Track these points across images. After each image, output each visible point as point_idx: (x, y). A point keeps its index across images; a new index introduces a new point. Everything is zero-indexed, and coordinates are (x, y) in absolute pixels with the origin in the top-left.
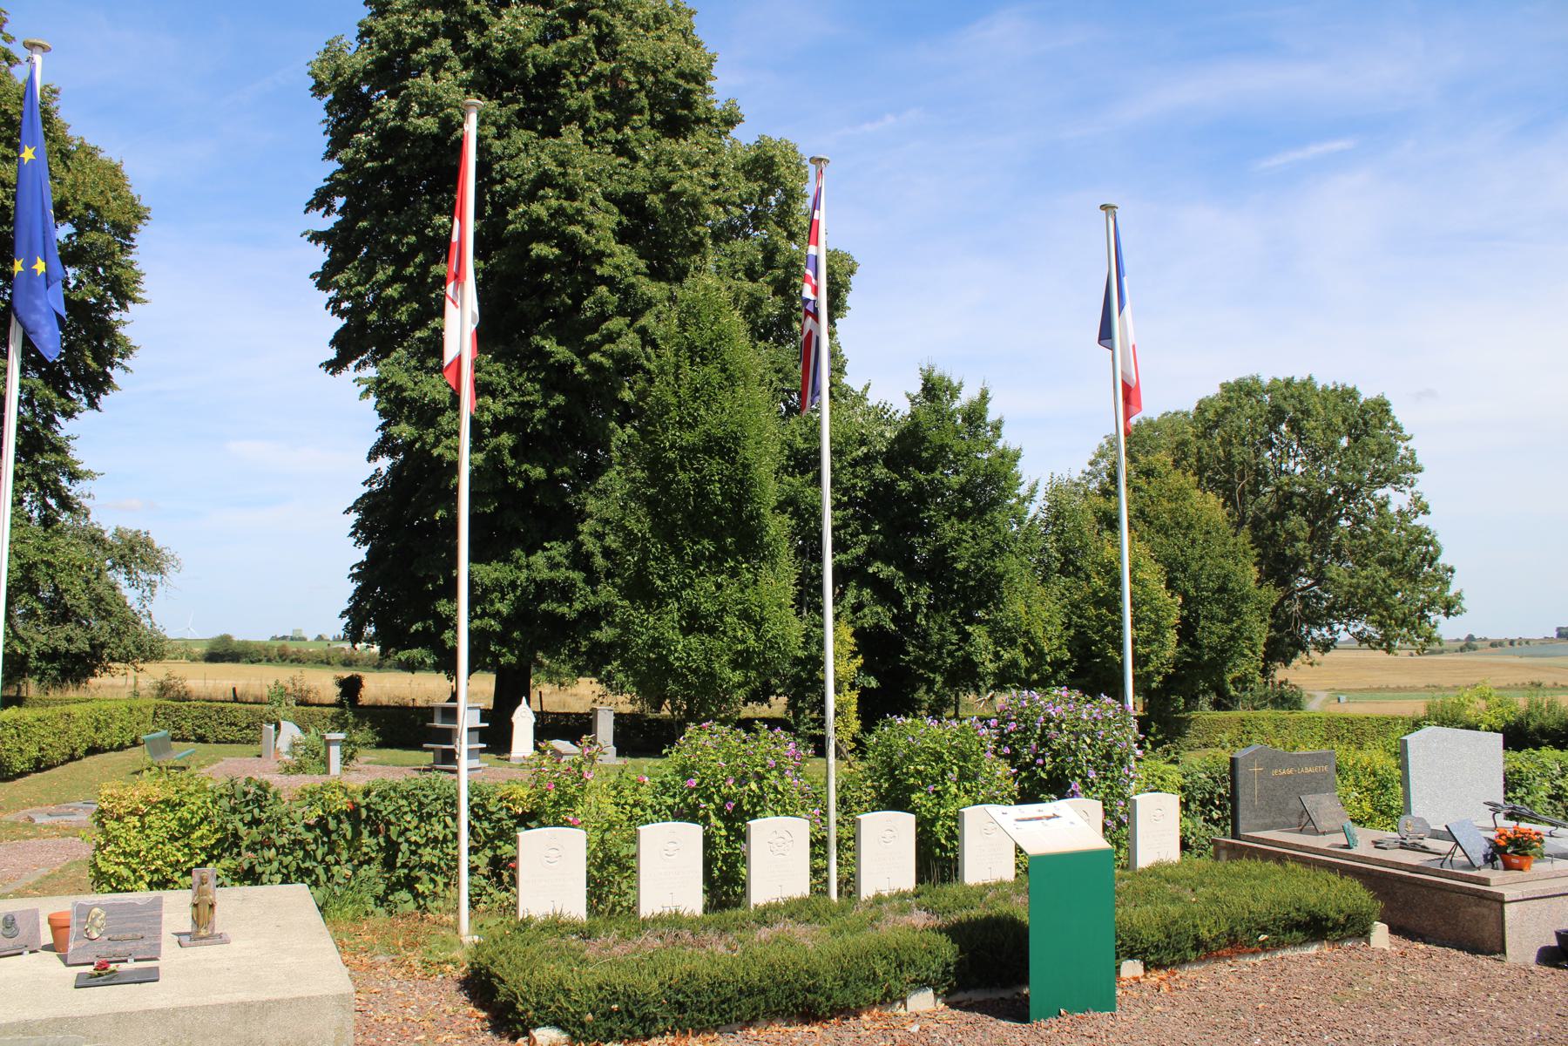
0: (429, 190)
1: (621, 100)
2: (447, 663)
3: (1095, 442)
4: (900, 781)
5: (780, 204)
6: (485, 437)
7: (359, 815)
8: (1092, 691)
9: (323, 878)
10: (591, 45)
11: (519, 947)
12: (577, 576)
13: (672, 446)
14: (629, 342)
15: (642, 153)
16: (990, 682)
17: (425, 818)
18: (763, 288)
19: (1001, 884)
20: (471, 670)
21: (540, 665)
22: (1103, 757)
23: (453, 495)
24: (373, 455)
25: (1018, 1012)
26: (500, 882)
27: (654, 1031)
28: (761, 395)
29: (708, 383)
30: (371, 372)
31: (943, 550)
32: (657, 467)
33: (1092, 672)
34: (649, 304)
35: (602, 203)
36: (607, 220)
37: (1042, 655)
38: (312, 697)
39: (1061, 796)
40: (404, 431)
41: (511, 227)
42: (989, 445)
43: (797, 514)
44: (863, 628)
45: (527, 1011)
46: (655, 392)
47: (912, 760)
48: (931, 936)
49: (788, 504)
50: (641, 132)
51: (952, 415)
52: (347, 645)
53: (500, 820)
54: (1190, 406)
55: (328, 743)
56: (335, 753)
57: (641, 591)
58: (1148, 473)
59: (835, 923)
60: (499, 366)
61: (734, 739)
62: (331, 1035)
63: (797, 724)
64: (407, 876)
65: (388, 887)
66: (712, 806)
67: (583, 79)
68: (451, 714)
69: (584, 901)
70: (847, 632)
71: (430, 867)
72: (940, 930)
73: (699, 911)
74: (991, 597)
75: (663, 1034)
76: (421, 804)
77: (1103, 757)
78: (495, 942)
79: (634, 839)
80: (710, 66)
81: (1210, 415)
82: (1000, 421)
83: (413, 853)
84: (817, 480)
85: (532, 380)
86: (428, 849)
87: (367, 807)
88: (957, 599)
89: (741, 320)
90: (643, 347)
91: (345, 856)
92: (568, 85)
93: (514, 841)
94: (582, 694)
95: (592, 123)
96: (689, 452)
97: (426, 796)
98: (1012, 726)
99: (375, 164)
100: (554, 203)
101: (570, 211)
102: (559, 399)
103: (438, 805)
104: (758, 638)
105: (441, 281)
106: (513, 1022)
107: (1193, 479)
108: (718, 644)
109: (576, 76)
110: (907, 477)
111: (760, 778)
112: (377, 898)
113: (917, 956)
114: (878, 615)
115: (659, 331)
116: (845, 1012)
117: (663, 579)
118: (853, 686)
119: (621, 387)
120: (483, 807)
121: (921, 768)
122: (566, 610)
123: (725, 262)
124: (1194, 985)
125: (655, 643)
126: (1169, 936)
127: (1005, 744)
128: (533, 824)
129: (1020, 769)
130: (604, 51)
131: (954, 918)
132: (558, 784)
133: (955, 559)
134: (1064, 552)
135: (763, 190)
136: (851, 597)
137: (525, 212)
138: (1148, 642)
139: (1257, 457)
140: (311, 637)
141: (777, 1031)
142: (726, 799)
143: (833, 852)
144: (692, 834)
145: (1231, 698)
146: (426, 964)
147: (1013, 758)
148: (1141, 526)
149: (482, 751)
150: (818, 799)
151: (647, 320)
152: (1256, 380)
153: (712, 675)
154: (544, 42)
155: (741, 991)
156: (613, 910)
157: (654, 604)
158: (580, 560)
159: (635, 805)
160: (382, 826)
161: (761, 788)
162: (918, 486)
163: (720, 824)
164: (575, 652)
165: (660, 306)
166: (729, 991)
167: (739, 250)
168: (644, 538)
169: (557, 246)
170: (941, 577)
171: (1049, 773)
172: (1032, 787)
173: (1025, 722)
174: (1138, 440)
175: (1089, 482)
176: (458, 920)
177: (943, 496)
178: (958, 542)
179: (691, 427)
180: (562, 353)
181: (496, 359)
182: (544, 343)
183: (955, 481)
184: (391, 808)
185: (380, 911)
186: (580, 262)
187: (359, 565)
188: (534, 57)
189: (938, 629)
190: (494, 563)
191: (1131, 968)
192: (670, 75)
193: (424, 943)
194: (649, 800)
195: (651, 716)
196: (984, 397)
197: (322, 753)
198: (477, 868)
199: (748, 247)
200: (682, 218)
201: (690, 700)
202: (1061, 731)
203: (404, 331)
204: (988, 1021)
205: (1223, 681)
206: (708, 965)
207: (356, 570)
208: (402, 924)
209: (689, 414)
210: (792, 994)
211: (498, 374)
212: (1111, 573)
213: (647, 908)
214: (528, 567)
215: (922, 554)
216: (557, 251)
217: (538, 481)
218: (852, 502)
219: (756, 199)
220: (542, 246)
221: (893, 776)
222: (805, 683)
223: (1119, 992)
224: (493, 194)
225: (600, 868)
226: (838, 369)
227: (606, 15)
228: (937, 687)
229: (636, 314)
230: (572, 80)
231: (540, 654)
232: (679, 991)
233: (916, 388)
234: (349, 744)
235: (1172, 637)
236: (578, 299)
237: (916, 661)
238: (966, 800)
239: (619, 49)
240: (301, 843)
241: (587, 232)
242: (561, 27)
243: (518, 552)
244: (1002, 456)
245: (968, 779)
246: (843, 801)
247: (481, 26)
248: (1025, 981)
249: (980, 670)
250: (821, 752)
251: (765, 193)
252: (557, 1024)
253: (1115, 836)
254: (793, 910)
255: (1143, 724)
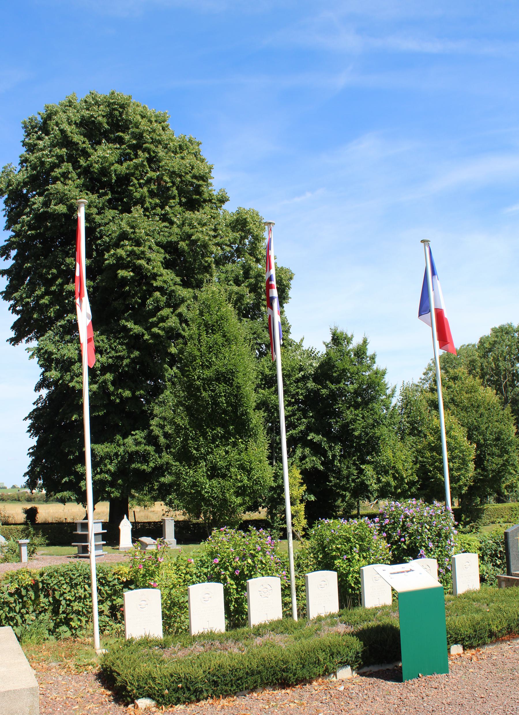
0: (62, 244)
1: (163, 192)
2: (82, 499)
3: (426, 362)
4: (328, 554)
5: (251, 243)
6: (98, 376)
7: (38, 586)
8: (429, 501)
9: (20, 621)
10: (145, 163)
11: (127, 655)
12: (151, 449)
13: (199, 378)
14: (173, 322)
15: (175, 220)
16: (376, 494)
17: (74, 586)
18: (244, 289)
19: (384, 607)
20: (95, 502)
21: (133, 497)
22: (436, 536)
23: (81, 407)
24: (38, 388)
25: (397, 676)
26: (116, 619)
27: (201, 697)
28: (245, 349)
29: (216, 343)
30: (34, 344)
31: (346, 425)
32: (191, 390)
33: (429, 489)
34: (183, 301)
35: (155, 247)
36: (158, 257)
37: (403, 479)
38: (11, 520)
39: (415, 558)
40: (54, 374)
41: (107, 262)
42: (369, 367)
43: (267, 410)
44: (306, 469)
45: (133, 690)
46: (188, 349)
47: (334, 542)
48: (348, 638)
49: (262, 405)
50: (175, 209)
51: (349, 352)
52: (29, 491)
53: (114, 585)
54: (476, 341)
55: (20, 545)
56: (24, 550)
57: (185, 456)
58: (455, 378)
59: (296, 633)
60: (104, 337)
61: (238, 536)
62: (27, 710)
63: (273, 522)
64: (65, 618)
65: (55, 624)
66: (228, 573)
67: (141, 181)
68: (85, 526)
69: (161, 627)
70: (297, 473)
71: (78, 613)
72: (352, 634)
73: (223, 630)
74: (374, 449)
75: (206, 699)
76: (71, 579)
77: (436, 536)
78: (114, 653)
79: (187, 593)
80: (210, 172)
81: (487, 345)
82: (374, 355)
83: (68, 605)
84: (276, 392)
85: (121, 344)
86: (76, 603)
87: (42, 582)
88: (356, 451)
89: (233, 309)
90: (181, 324)
91: (31, 609)
92: (134, 185)
93: (122, 597)
94: (156, 511)
95: (147, 205)
96: (208, 381)
97: (74, 575)
98: (387, 521)
99: (33, 232)
100: (129, 248)
101: (138, 252)
102: (137, 353)
103: (81, 579)
104: (249, 479)
105: (72, 293)
106: (126, 696)
107: (478, 380)
108: (228, 483)
109: (138, 180)
110: (325, 387)
111: (253, 556)
112: (50, 630)
113: (341, 649)
114: (314, 462)
115: (189, 315)
116: (303, 681)
117: (197, 450)
118: (302, 501)
119: (170, 346)
120: (104, 578)
121: (339, 546)
122: (145, 467)
123: (223, 276)
124: (490, 656)
125: (194, 485)
126: (475, 631)
127: (384, 531)
128: (132, 587)
129: (392, 544)
130: (153, 166)
131: (360, 627)
132: (144, 565)
133: (353, 430)
134: (411, 423)
135: (241, 237)
136: (299, 452)
137: (114, 254)
138: (459, 469)
139: (512, 366)
140: (9, 486)
141: (268, 693)
142: (235, 569)
143: (293, 594)
144: (218, 588)
145: (505, 496)
146: (78, 666)
147: (388, 538)
148: (452, 407)
149: (104, 545)
150: (284, 565)
151: (182, 309)
152: (510, 326)
153: (225, 500)
154: (120, 162)
155: (247, 673)
156: (177, 632)
157: (193, 463)
158: (152, 440)
159: (187, 573)
160: (51, 592)
161: (254, 562)
162: (332, 391)
163: (232, 582)
164: (151, 490)
165: (189, 302)
166: (241, 674)
167: (230, 270)
168: (186, 428)
169: (131, 271)
170: (346, 440)
171: (408, 546)
172: (399, 554)
173: (394, 518)
174: (447, 363)
175: (424, 384)
176: (94, 641)
177: (346, 396)
178: (355, 420)
179: (208, 367)
180: (137, 329)
181: (101, 334)
182: (126, 324)
183: (351, 388)
184: (55, 582)
185: (52, 637)
186: (144, 279)
187: (32, 448)
188: (115, 171)
189: (346, 467)
190: (105, 444)
191: (456, 649)
192: (188, 177)
193: (76, 655)
194: (194, 571)
195: (194, 521)
196: (365, 342)
197: (17, 550)
198: (103, 611)
199: (234, 268)
200: (198, 253)
201: (214, 514)
202: (413, 522)
203: (52, 322)
204: (381, 683)
205: (500, 487)
206: (229, 660)
207: (31, 451)
208: (64, 644)
209: (207, 361)
210: (275, 673)
211: (104, 342)
212: (437, 431)
213: (195, 630)
214: (124, 444)
215: (336, 428)
216: (132, 274)
217: (127, 398)
218: (297, 402)
219: (238, 242)
220: (124, 271)
221: (324, 552)
222: (276, 501)
223: (450, 663)
224: (96, 246)
225: (170, 609)
226: (286, 330)
227: (152, 147)
228: (347, 499)
229: (176, 307)
230: (136, 182)
231: (133, 491)
232: (214, 675)
233: (329, 339)
234: (32, 545)
235: (472, 465)
236: (144, 299)
237: (335, 485)
238: (364, 562)
239: (161, 164)
240: (7, 603)
241: (148, 263)
242: (128, 154)
243: (118, 437)
244: (376, 373)
245: (364, 551)
246: (298, 566)
247: (86, 154)
248: (400, 660)
249: (370, 488)
250: (285, 537)
251: (242, 238)
252: (149, 696)
253: (445, 577)
254: (274, 627)
255: (457, 514)
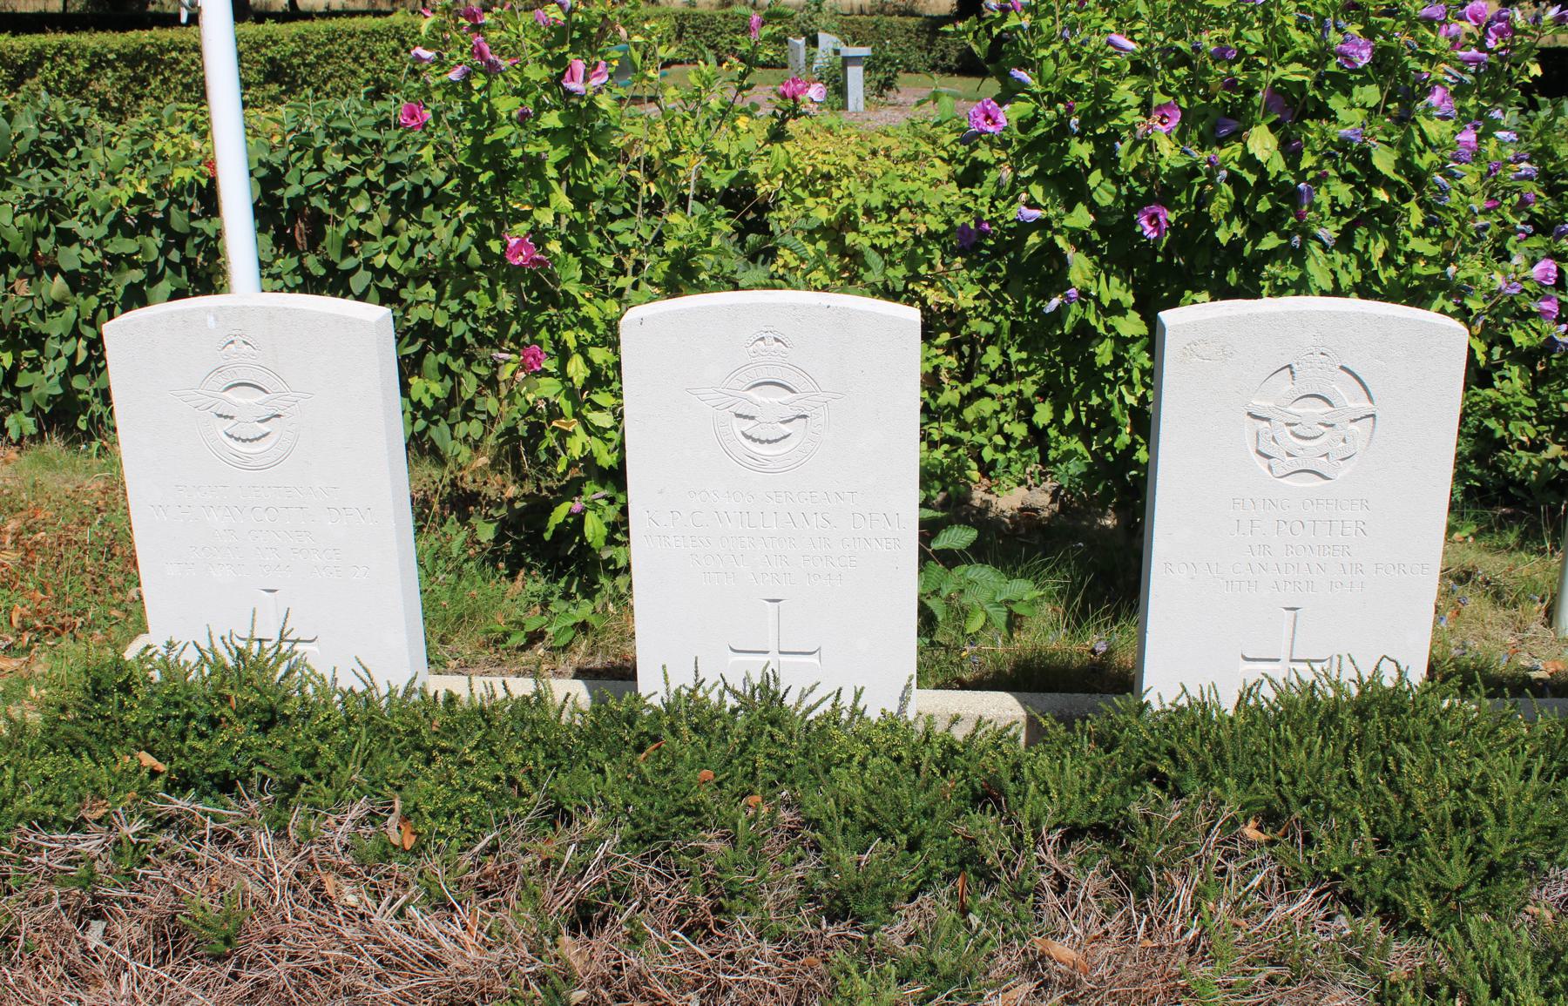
111: (1295, 111)
161: (1290, 150)
